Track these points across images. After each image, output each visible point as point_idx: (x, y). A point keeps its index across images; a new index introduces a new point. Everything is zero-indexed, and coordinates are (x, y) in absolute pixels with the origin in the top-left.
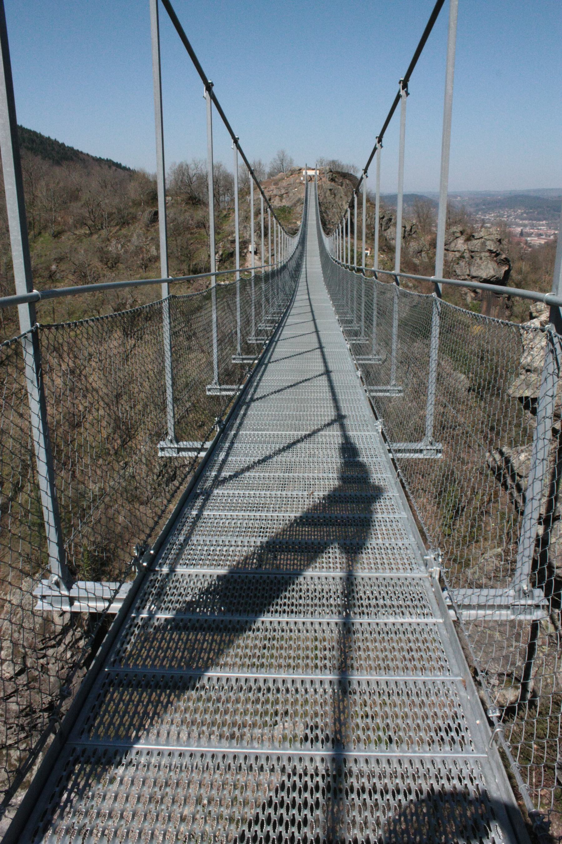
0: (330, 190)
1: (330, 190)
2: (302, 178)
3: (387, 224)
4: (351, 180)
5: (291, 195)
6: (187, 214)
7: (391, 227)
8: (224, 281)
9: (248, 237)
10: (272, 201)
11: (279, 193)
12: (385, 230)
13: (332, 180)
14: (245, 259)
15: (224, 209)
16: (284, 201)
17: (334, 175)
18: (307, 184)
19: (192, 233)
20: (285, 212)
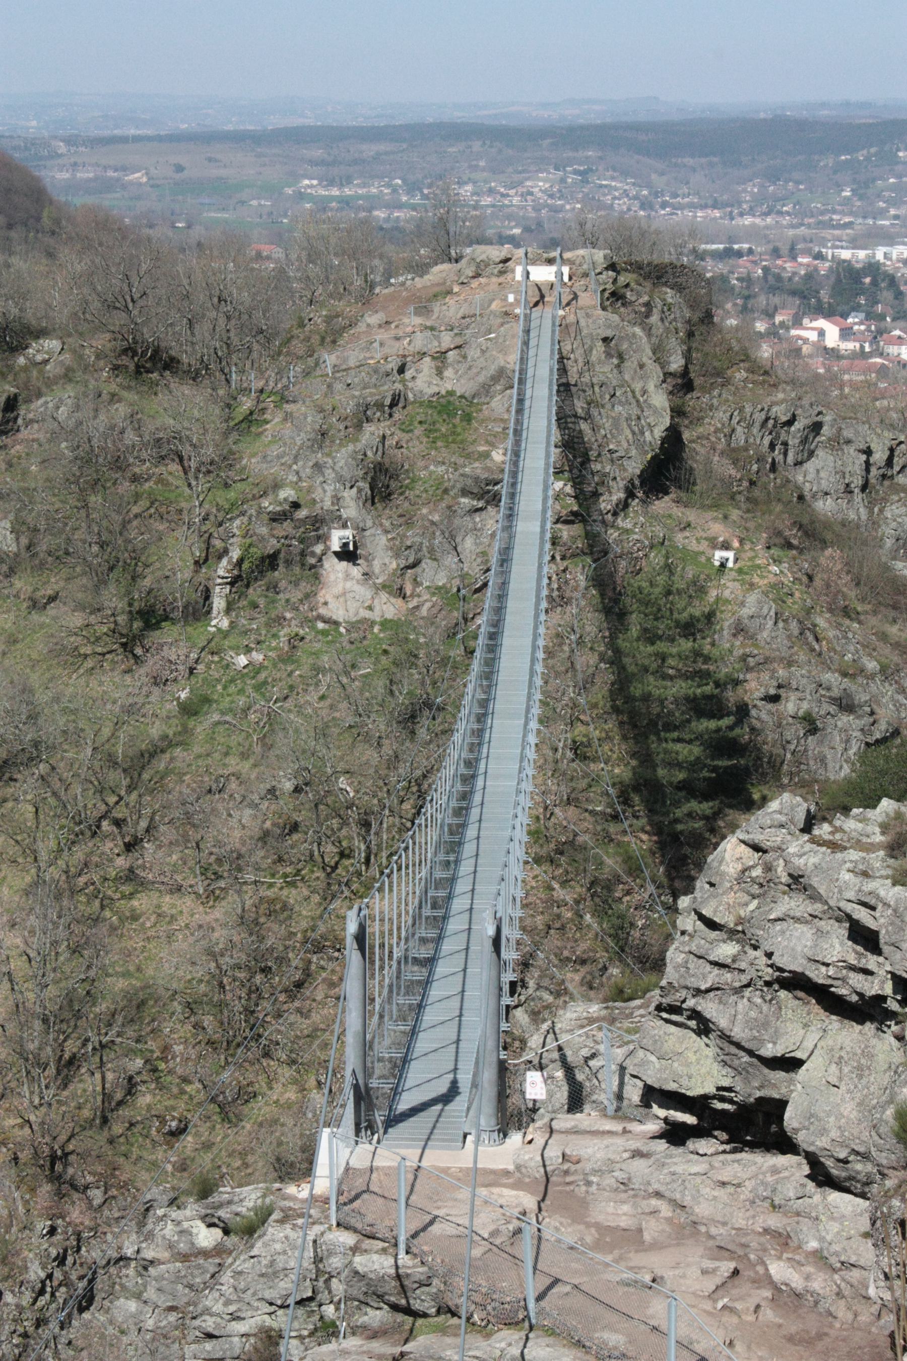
0: (605, 340)
1: (605, 340)
2: (511, 298)
3: (804, 441)
4: (679, 288)
5: (473, 353)
6: (121, 410)
7: (820, 453)
8: (248, 650)
9: (327, 504)
10: (408, 374)
11: (434, 347)
12: (799, 463)
13: (615, 298)
14: (317, 577)
15: (247, 391)
16: (448, 373)
17: (622, 279)
18: (528, 318)
19: (135, 479)
20: (451, 414)
